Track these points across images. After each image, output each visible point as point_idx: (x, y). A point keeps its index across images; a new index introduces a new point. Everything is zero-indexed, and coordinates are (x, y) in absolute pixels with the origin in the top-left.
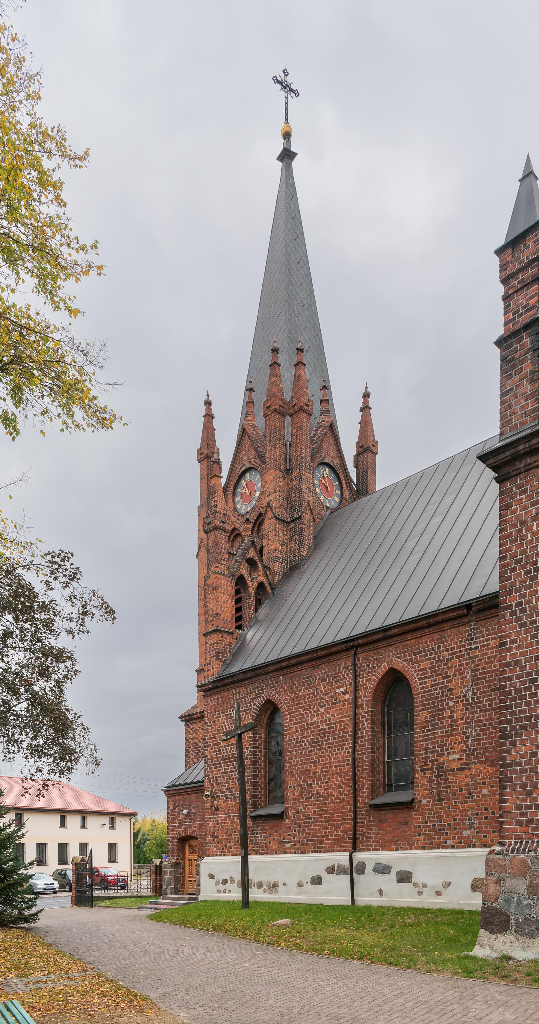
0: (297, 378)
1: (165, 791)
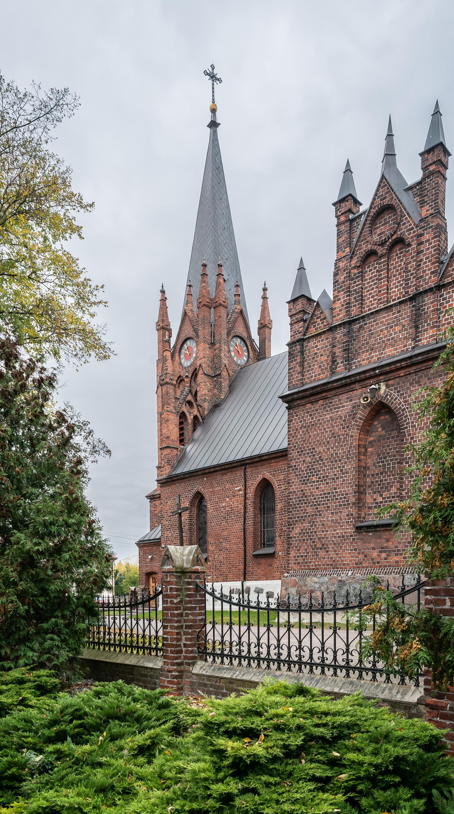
1: (137, 544)
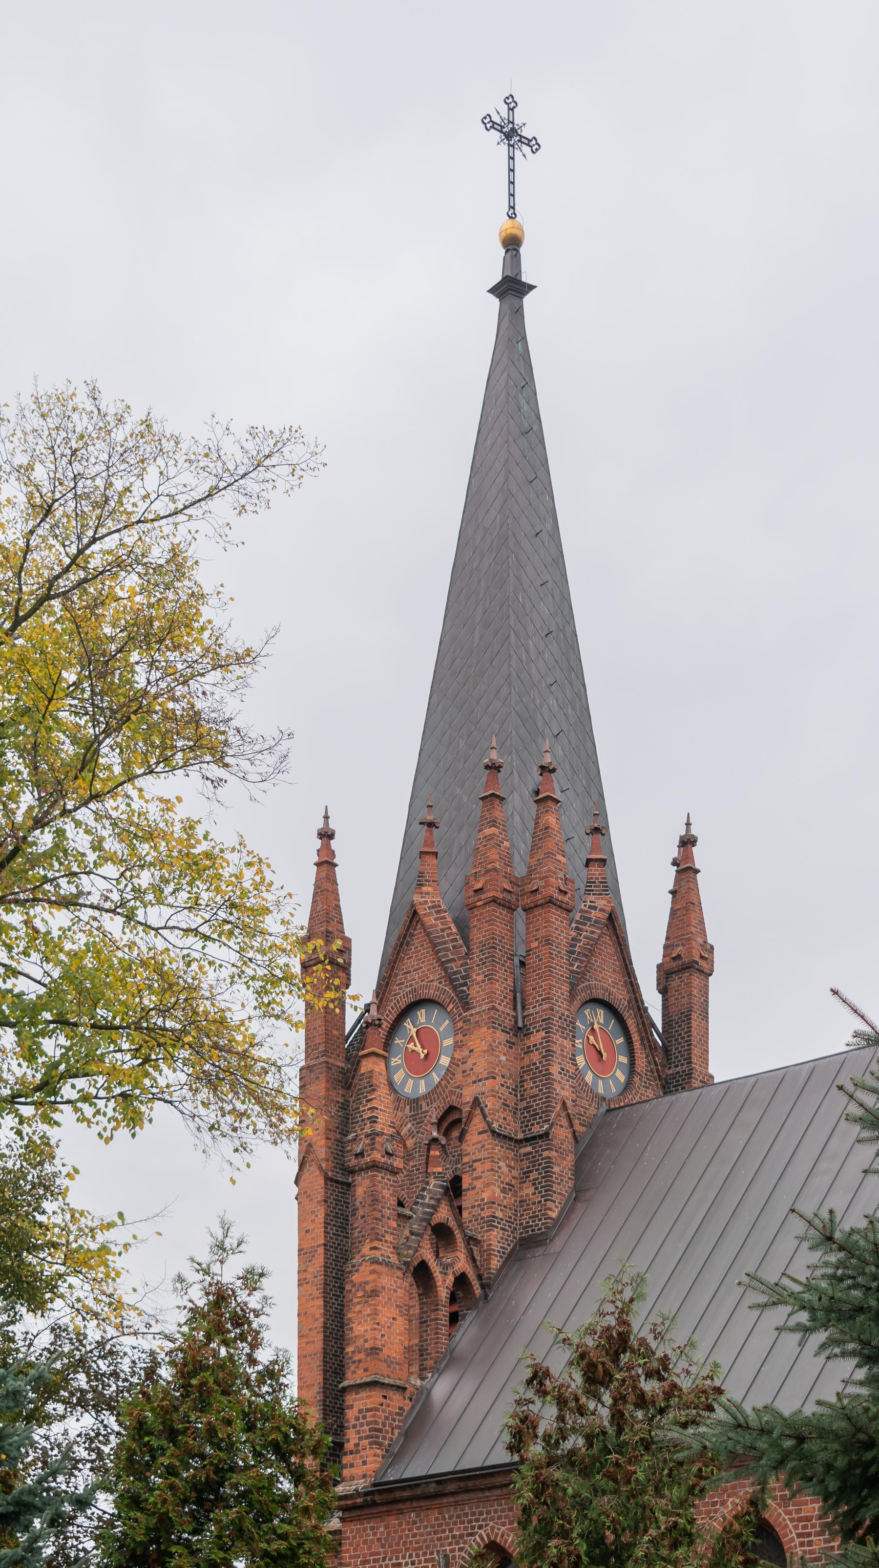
0: (541, 833)
